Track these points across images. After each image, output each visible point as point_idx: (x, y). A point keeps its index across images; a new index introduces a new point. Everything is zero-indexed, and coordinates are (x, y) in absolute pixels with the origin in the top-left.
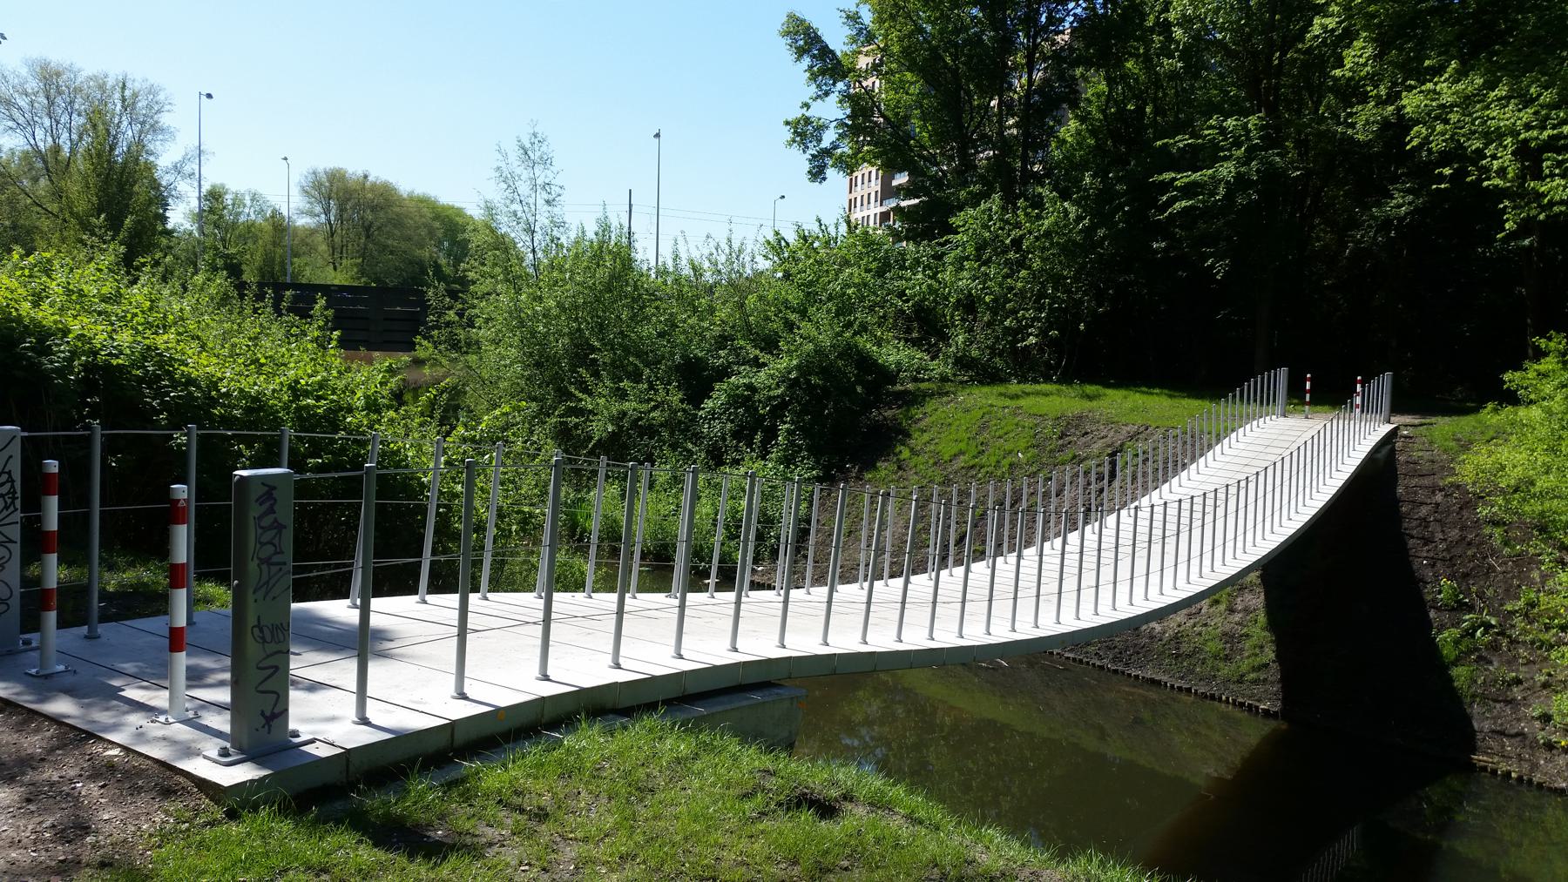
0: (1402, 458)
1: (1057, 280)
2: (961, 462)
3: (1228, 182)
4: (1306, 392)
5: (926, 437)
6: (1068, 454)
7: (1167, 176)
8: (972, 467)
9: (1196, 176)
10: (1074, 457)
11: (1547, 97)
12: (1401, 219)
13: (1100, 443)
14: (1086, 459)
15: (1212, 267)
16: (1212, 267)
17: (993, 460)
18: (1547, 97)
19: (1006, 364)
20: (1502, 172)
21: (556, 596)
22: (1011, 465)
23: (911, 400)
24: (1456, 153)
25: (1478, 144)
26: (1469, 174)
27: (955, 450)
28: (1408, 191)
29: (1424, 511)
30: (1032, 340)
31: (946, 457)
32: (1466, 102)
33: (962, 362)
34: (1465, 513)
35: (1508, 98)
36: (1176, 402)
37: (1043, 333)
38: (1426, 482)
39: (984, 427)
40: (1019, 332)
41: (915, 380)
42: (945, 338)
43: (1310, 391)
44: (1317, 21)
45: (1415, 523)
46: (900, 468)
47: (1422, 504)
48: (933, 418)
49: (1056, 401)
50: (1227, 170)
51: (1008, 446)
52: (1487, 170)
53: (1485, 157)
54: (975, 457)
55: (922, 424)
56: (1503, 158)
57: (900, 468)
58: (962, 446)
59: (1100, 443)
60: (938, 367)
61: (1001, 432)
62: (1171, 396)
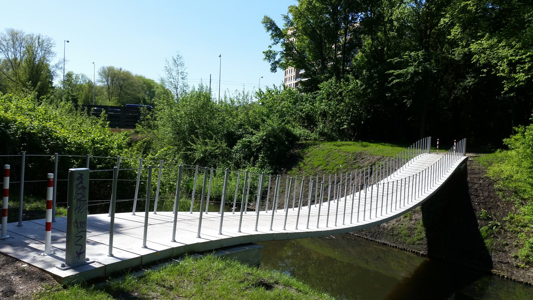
0: (469, 168)
2: (320, 168)
5: (309, 159)
6: (357, 165)
8: (324, 170)
10: (359, 166)
13: (368, 162)
15: (406, 102)
16: (406, 102)
17: (331, 167)
20: (503, 71)
22: (337, 169)
28: (473, 77)
29: (476, 186)
30: (345, 126)
31: (316, 166)
32: (491, 47)
33: (322, 134)
37: (349, 124)
38: (477, 176)
39: (328, 156)
40: (342, 124)
41: (306, 140)
42: (316, 126)
43: (439, 145)
44: (442, 19)
46: (300, 170)
47: (476, 183)
49: (353, 147)
50: (411, 69)
51: (337, 163)
52: (498, 70)
53: (498, 66)
56: (504, 66)
57: (300, 170)
58: (321, 162)
59: (368, 162)
60: (313, 135)
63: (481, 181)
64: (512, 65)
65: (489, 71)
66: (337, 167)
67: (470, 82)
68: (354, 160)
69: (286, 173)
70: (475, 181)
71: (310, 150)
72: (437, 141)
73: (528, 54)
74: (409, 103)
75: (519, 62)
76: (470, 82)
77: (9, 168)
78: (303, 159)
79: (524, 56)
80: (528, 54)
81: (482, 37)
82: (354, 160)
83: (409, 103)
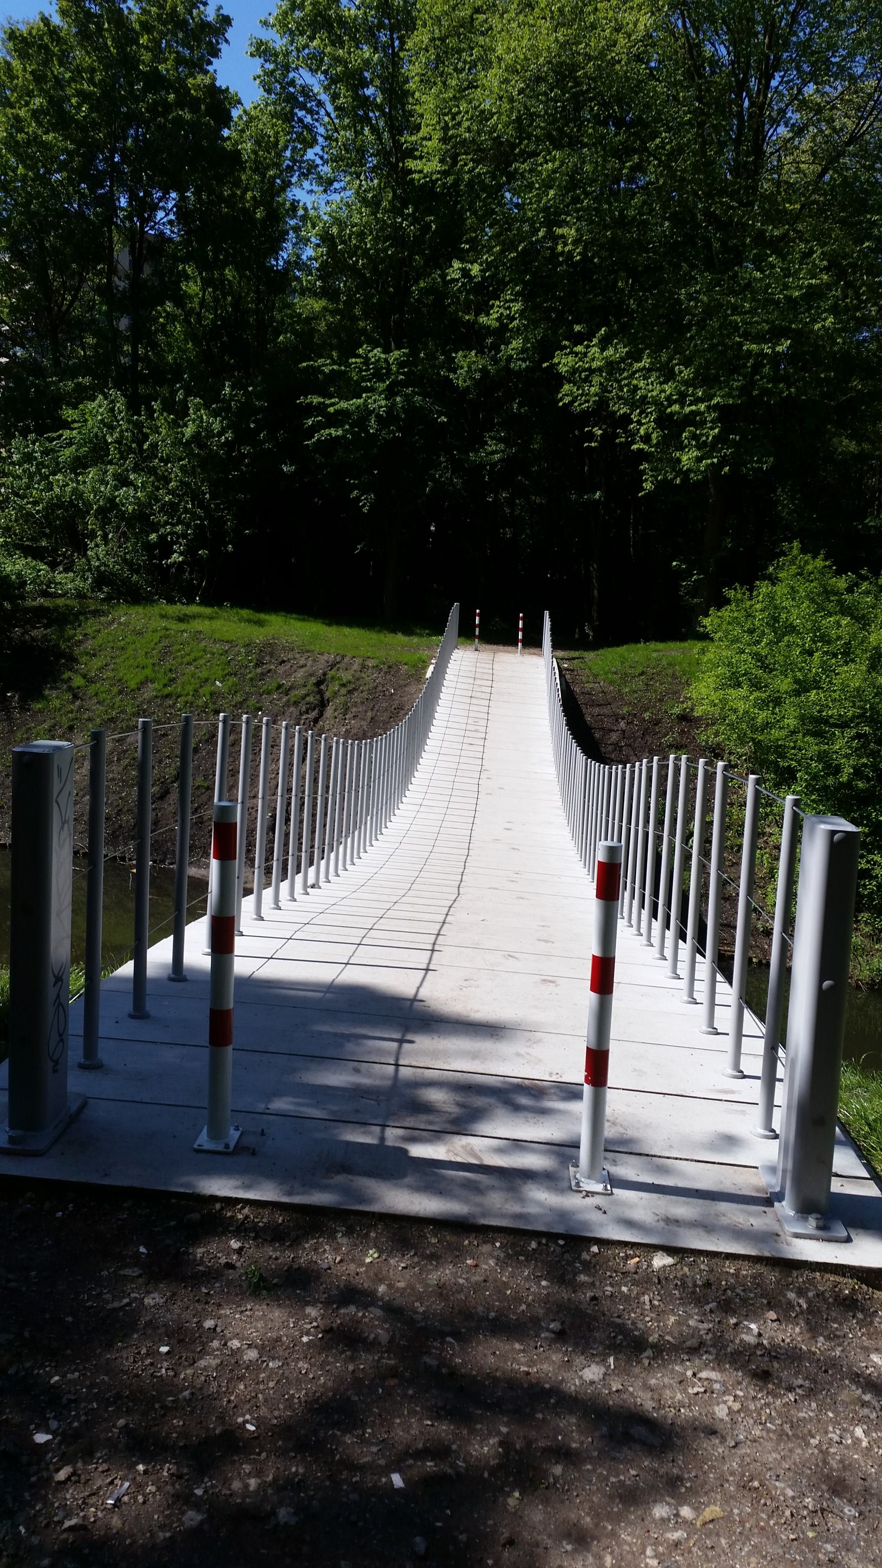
0: (577, 689)
1: (196, 496)
2: (149, 691)
3: (378, 416)
4: (475, 626)
5: (97, 663)
6: (270, 683)
7: (316, 400)
8: (168, 696)
9: (344, 405)
10: (279, 686)
11: (687, 373)
12: (495, 464)
13: (300, 673)
14: (291, 688)
15: (358, 499)
16: (358, 499)
17: (190, 688)
18: (687, 373)
19: (149, 581)
20: (646, 439)
21: (759, 1082)
22: (212, 694)
23: (63, 619)
24: (600, 411)
25: (624, 410)
26: (618, 436)
27: (141, 677)
28: (500, 440)
29: (614, 737)
30: (176, 558)
31: (133, 685)
32: (611, 367)
33: (102, 579)
34: (647, 738)
35: (649, 370)
36: (382, 636)
37: (190, 551)
38: (606, 710)
39: (166, 653)
40: (165, 547)
41: (45, 594)
42: (82, 549)
43: (479, 626)
44: (456, 264)
45: (610, 748)
46: (76, 697)
47: (611, 730)
48: (99, 640)
49: (230, 627)
50: (378, 402)
51: (204, 674)
52: (633, 434)
53: (632, 422)
54: (165, 686)
55: (89, 645)
56: (646, 425)
57: (76, 697)
58: (148, 672)
59: (300, 673)
60: (66, 581)
61: (187, 659)
62: (299, 620)
63: (622, 724)
64: (672, 427)
65: (608, 439)
66: (206, 689)
67: (493, 453)
68: (257, 665)
69: (23, 709)
70: (607, 723)
71: (89, 631)
72: (518, 619)
73: (715, 401)
74: (366, 502)
75: (690, 420)
76: (493, 453)
77: (196, 1491)
78: (76, 661)
79: (702, 407)
80: (715, 401)
81: (589, 336)
82: (257, 665)
83: (366, 502)
